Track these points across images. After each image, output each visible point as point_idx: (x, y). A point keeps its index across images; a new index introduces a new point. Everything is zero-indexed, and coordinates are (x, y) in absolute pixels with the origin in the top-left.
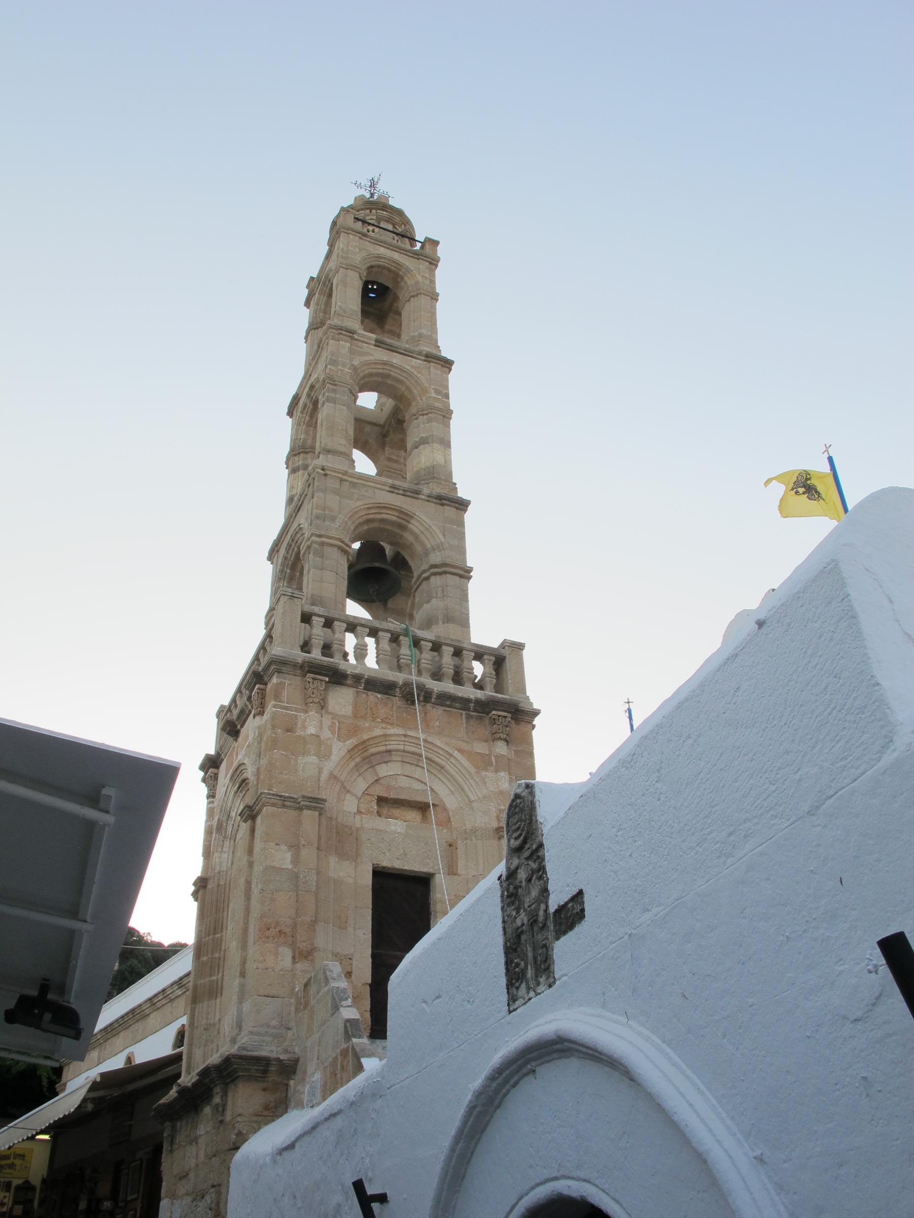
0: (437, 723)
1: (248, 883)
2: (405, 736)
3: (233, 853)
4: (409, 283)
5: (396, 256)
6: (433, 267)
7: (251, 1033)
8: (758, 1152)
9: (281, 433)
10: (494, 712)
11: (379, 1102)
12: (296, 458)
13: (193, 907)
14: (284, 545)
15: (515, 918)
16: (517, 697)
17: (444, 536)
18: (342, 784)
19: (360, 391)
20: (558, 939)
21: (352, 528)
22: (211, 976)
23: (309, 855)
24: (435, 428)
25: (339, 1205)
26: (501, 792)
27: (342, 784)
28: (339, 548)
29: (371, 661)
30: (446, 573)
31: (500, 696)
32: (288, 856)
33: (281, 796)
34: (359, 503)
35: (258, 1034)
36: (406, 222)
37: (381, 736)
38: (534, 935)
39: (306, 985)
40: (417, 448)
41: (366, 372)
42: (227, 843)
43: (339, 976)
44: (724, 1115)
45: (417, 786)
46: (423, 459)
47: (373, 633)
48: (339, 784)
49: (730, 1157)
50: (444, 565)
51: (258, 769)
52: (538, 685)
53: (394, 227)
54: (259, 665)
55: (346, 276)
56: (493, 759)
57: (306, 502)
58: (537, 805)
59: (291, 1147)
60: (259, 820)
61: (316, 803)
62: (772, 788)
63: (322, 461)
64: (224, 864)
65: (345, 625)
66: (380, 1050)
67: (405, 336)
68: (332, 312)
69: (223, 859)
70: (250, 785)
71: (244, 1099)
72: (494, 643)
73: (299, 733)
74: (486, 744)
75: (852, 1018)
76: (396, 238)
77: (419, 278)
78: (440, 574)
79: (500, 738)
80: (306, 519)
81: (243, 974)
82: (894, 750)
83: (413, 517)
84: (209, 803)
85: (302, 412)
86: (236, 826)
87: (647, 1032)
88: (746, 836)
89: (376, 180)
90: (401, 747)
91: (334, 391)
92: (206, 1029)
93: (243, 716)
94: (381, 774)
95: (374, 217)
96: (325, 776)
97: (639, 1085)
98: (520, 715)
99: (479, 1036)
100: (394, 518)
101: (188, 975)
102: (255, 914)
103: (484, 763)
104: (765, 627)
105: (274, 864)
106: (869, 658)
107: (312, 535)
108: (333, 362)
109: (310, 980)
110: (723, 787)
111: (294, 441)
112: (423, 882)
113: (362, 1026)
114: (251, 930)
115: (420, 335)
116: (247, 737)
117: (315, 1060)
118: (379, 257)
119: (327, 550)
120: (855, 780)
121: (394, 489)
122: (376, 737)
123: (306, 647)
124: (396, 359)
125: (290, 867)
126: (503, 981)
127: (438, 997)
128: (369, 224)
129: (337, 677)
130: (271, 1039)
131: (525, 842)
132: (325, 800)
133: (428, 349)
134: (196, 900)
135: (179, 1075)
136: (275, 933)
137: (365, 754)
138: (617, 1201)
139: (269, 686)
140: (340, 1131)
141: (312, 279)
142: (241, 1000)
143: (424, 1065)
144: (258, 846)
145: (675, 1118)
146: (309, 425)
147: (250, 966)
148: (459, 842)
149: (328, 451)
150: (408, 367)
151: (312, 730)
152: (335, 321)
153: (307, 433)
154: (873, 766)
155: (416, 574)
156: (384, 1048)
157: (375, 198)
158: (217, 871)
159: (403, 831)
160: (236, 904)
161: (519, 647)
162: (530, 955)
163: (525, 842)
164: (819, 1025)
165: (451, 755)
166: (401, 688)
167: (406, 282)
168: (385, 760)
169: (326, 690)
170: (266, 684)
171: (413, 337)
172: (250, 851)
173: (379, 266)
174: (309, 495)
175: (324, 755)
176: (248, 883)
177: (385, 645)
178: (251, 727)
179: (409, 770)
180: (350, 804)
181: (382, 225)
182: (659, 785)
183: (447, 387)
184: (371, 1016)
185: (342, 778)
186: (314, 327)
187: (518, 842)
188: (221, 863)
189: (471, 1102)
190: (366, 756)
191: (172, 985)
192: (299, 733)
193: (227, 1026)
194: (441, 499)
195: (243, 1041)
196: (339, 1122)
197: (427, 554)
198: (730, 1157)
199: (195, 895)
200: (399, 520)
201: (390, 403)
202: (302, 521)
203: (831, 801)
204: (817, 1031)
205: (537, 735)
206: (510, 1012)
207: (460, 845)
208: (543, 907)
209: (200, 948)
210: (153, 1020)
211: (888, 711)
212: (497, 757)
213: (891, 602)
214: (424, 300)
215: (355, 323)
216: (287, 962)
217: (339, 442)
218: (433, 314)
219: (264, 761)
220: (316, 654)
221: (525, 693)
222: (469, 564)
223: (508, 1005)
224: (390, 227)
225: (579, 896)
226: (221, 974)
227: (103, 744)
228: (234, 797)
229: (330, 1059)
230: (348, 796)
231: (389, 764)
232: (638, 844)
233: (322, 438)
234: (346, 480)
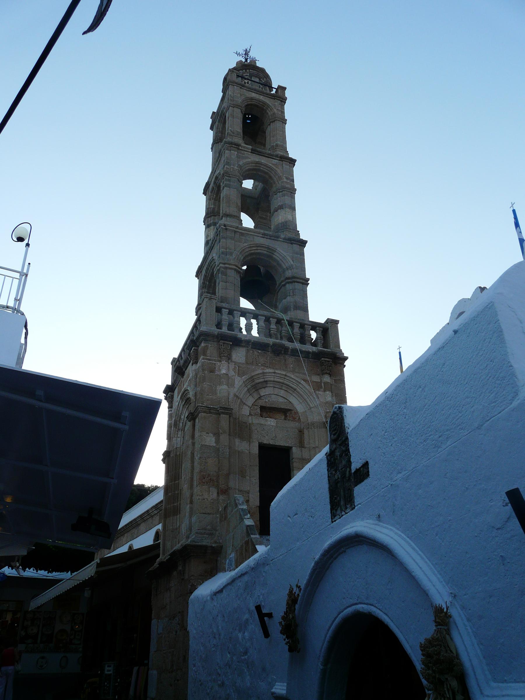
1: (193, 454)
2: (274, 373)
3: (183, 437)
4: (269, 114)
5: (261, 98)
6: (283, 103)
7: (197, 533)
8: (450, 592)
9: (200, 205)
10: (323, 359)
11: (267, 568)
12: (210, 219)
13: (163, 467)
14: (205, 268)
15: (335, 475)
16: (335, 350)
17: (293, 261)
18: (241, 400)
19: (244, 180)
20: (356, 486)
21: (242, 258)
22: (174, 503)
23: (224, 438)
24: (287, 199)
25: (247, 620)
26: (327, 402)
27: (241, 400)
28: (235, 270)
29: (255, 333)
30: (294, 282)
31: (326, 350)
32: (213, 439)
33: (208, 407)
35: (201, 534)
36: (267, 76)
37: (261, 373)
38: (344, 482)
39: (225, 508)
40: (277, 211)
41: (247, 168)
42: (180, 433)
43: (243, 503)
44: (436, 573)
45: (281, 400)
47: (256, 317)
48: (240, 400)
49: (439, 593)
50: (294, 277)
51: (196, 393)
52: (347, 343)
53: (260, 80)
54: (194, 336)
55: (233, 111)
56: (323, 384)
57: (216, 245)
58: (345, 418)
59: (221, 591)
60: (197, 420)
61: (227, 411)
62: (460, 415)
63: (224, 221)
64: (179, 443)
65: (240, 313)
66: (265, 541)
67: (268, 146)
68: (226, 133)
70: (192, 401)
71: (195, 567)
72: (322, 321)
74: (319, 377)
75: (496, 528)
76: (261, 86)
77: (275, 110)
78: (291, 282)
79: (326, 373)
80: (217, 254)
81: (191, 502)
82: (518, 399)
84: (169, 411)
85: (211, 192)
86: (184, 424)
87: (400, 533)
88: (447, 438)
89: (248, 50)
90: (272, 379)
91: (229, 181)
92: (172, 531)
93: (186, 364)
95: (248, 74)
96: (231, 396)
97: (396, 558)
98: (338, 360)
99: (317, 534)
100: (265, 252)
101: (162, 501)
102: (197, 470)
103: (317, 387)
104: (457, 334)
105: (206, 444)
106: (508, 353)
107: (220, 263)
108: (228, 163)
109: (227, 505)
110: (437, 413)
111: (207, 209)
112: (286, 451)
113: (18, 367)
114: (195, 478)
115: (277, 145)
116: (189, 375)
117: (231, 547)
118: (252, 99)
119: (229, 271)
120: (500, 412)
121: (264, 235)
122: (258, 374)
123: (219, 325)
124: (264, 160)
125: (214, 445)
126: (329, 507)
127: (296, 514)
128: (245, 79)
129: (237, 342)
130: (207, 536)
131: (339, 436)
132: (232, 409)
133: (282, 154)
134: (164, 463)
135: (158, 556)
136: (207, 480)
138: (386, 614)
139: (200, 348)
140: (247, 582)
141: (214, 113)
142: (190, 517)
143: (289, 549)
144: (197, 434)
145: (413, 574)
146: (215, 200)
147: (195, 498)
148: (305, 430)
149: (227, 215)
150: (270, 165)
151: (224, 371)
152: (229, 139)
153: (214, 204)
154: (509, 406)
155: (278, 283)
156: (268, 540)
157: (248, 61)
159: (275, 424)
160: (186, 465)
161: (336, 322)
162: (342, 493)
163: (339, 436)
164: (481, 531)
167: (267, 113)
168: (264, 386)
169: (231, 349)
171: (273, 146)
172: (193, 437)
174: (218, 241)
175: (231, 385)
176: (193, 454)
177: (262, 323)
178: (191, 370)
179: (277, 391)
180: (246, 411)
181: (253, 79)
182: (405, 411)
183: (293, 176)
184: (260, 523)
185: (241, 397)
186: (216, 141)
187: (335, 437)
189: (313, 567)
190: (255, 386)
191: (152, 508)
193: (184, 529)
194: (291, 240)
195: (193, 537)
196: (246, 578)
197: (284, 271)
198: (439, 593)
199: (164, 460)
200: (268, 253)
201: (260, 185)
202: (214, 255)
203: (488, 422)
204: (480, 533)
205: (347, 371)
206: (332, 522)
207: (306, 432)
208: (348, 469)
209: (167, 488)
210: (142, 527)
211: (516, 379)
212: (324, 383)
213: (521, 323)
214: (278, 124)
215: (240, 141)
216: (215, 494)
217: (232, 210)
218: (284, 132)
219: (199, 389)
220: (225, 330)
221: (339, 347)
223: (332, 519)
224: (257, 80)
225: (366, 465)
227: (122, 391)
228: (183, 408)
229: (240, 546)
230: (245, 407)
232: (396, 439)
233: (224, 208)
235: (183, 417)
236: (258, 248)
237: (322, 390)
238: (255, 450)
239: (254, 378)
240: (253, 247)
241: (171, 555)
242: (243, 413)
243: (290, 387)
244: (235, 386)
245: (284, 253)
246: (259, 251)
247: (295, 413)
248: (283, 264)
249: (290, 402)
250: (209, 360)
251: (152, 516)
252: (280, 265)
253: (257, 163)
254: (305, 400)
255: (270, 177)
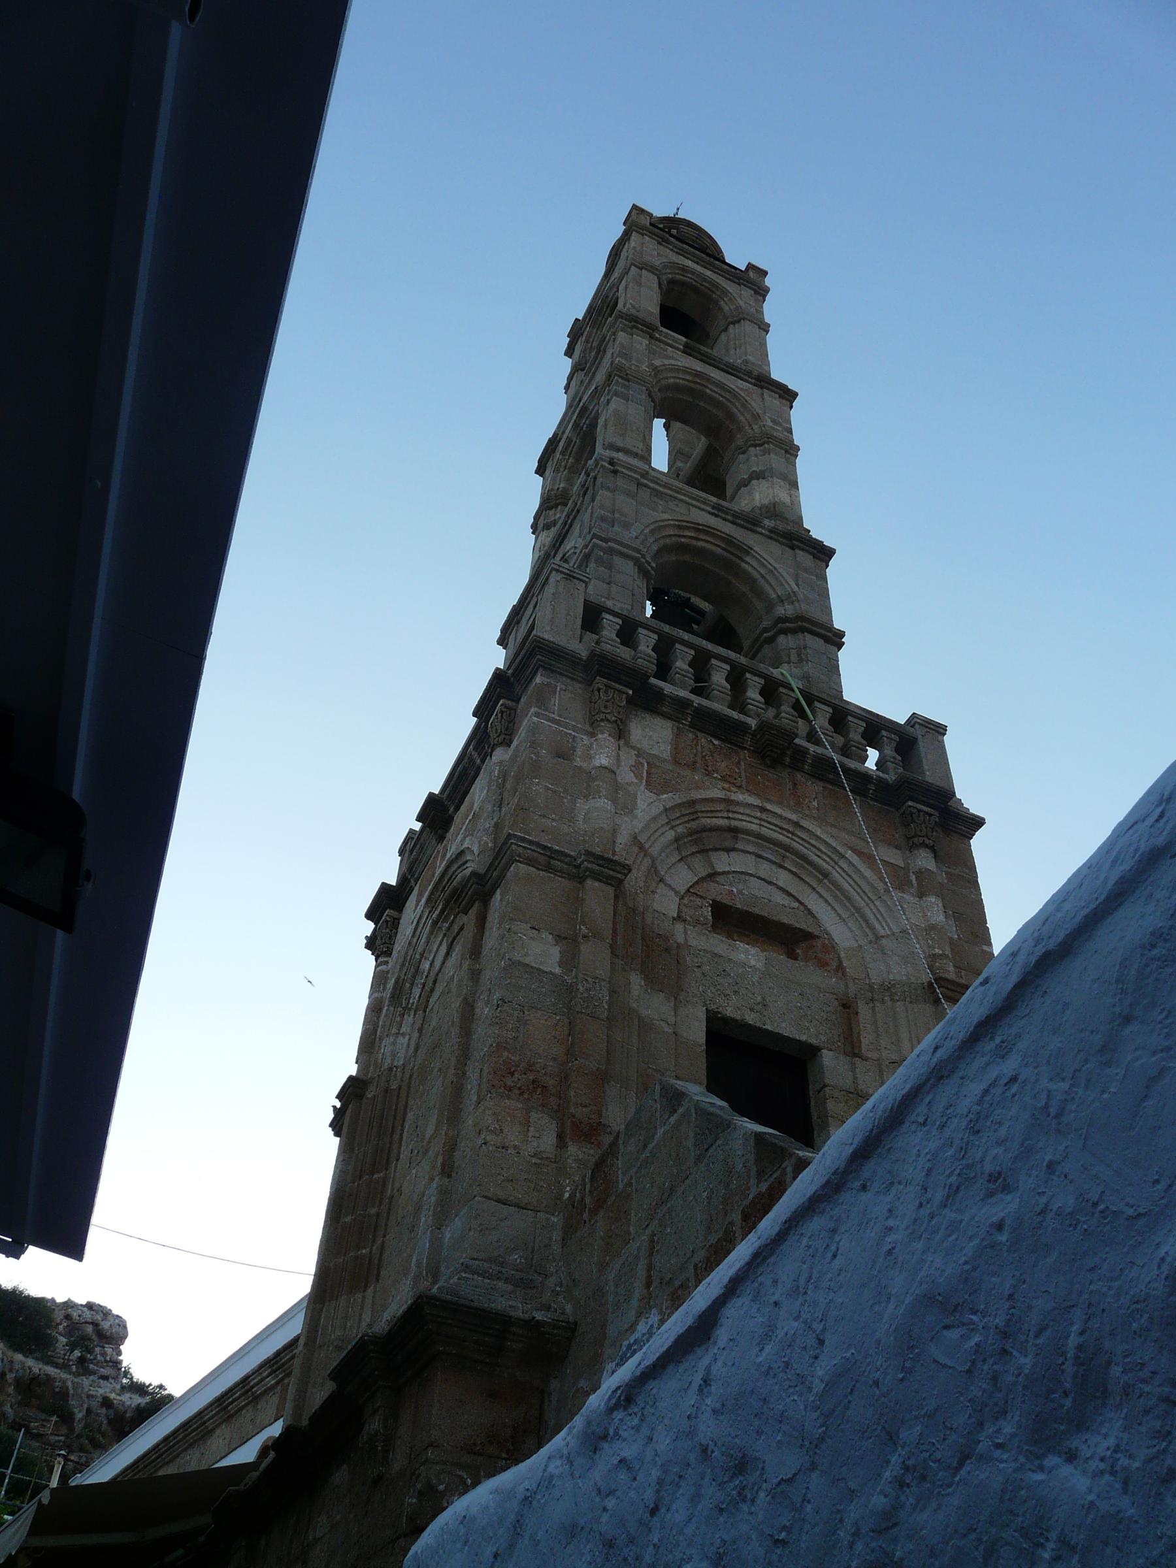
0: (815, 804)
2: (763, 809)
3: (420, 1031)
4: (726, 308)
7: (466, 1268)
10: (910, 803)
12: (551, 512)
22: (358, 1248)
23: (595, 957)
28: (636, 562)
32: (555, 952)
33: (545, 848)
34: (666, 516)
42: (409, 1019)
46: (757, 497)
56: (913, 878)
64: (401, 1055)
69: (398, 1048)
71: (448, 1409)
73: (578, 762)
77: (742, 303)
78: (794, 631)
79: (927, 846)
83: (748, 553)
90: (754, 827)
91: (627, 388)
94: (720, 868)
96: (623, 839)
100: (719, 551)
105: (527, 960)
119: (617, 560)
122: (712, 800)
125: (557, 970)
130: (510, 1288)
134: (336, 1135)
137: (694, 825)
141: (577, 320)
142: (439, 1224)
151: (602, 760)
158: (386, 1066)
159: (760, 965)
165: (843, 856)
166: (754, 735)
167: (720, 309)
168: (727, 844)
170: (518, 701)
173: (683, 284)
175: (627, 807)
179: (765, 869)
180: (666, 903)
185: (655, 851)
188: (394, 1055)
190: (701, 836)
192: (578, 762)
207: (863, 1008)
216: (548, 1141)
222: (838, 624)
226: (379, 1241)
228: (431, 933)
230: (662, 889)
231: (732, 854)
234: (646, 486)
235: (426, 965)
236: (701, 537)
237: (912, 891)
238: (697, 1032)
239: (698, 807)
240: (688, 528)
241: (335, 1375)
242: (656, 906)
243: (810, 863)
244: (638, 812)
245: (772, 561)
246: (701, 544)
247: (824, 945)
248: (767, 587)
249: (810, 912)
250: (554, 721)
251: (256, 1399)
252: (759, 593)
253: (698, 374)
254: (858, 910)
255: (731, 416)
